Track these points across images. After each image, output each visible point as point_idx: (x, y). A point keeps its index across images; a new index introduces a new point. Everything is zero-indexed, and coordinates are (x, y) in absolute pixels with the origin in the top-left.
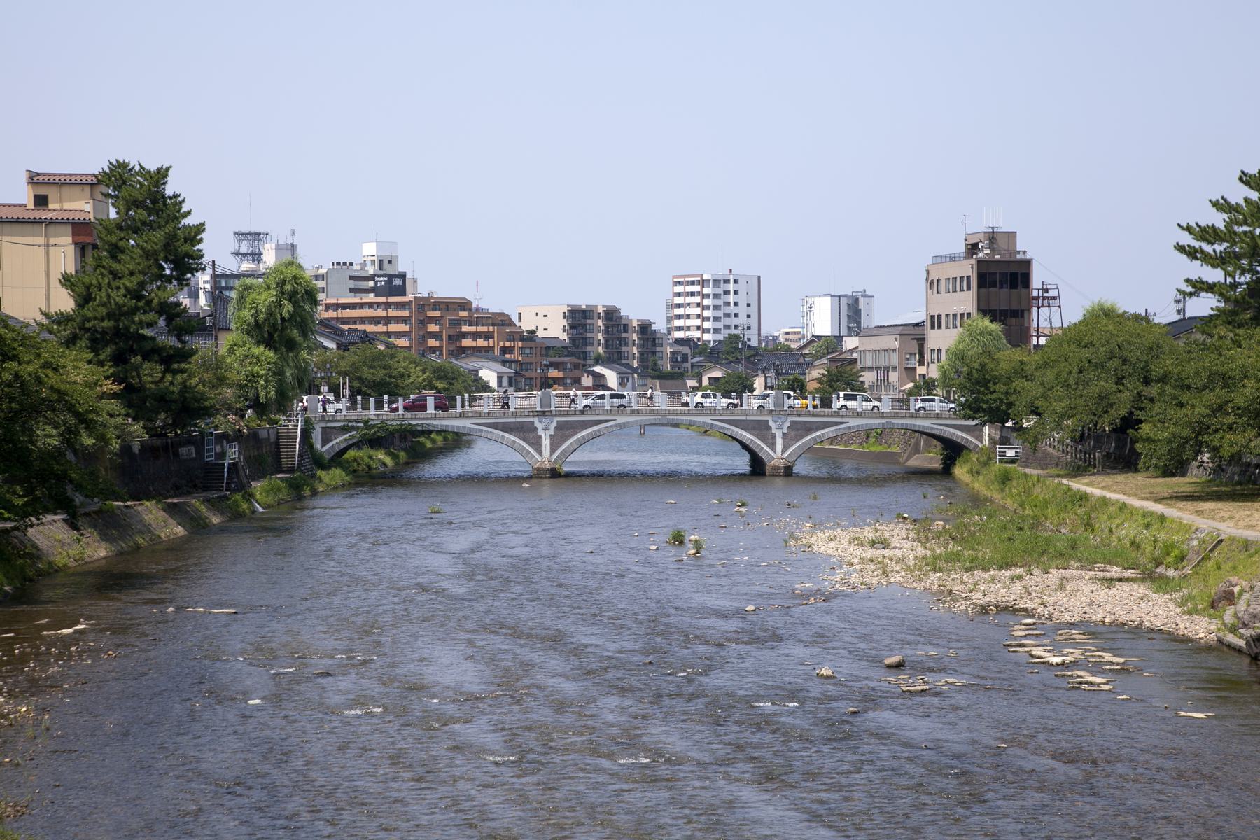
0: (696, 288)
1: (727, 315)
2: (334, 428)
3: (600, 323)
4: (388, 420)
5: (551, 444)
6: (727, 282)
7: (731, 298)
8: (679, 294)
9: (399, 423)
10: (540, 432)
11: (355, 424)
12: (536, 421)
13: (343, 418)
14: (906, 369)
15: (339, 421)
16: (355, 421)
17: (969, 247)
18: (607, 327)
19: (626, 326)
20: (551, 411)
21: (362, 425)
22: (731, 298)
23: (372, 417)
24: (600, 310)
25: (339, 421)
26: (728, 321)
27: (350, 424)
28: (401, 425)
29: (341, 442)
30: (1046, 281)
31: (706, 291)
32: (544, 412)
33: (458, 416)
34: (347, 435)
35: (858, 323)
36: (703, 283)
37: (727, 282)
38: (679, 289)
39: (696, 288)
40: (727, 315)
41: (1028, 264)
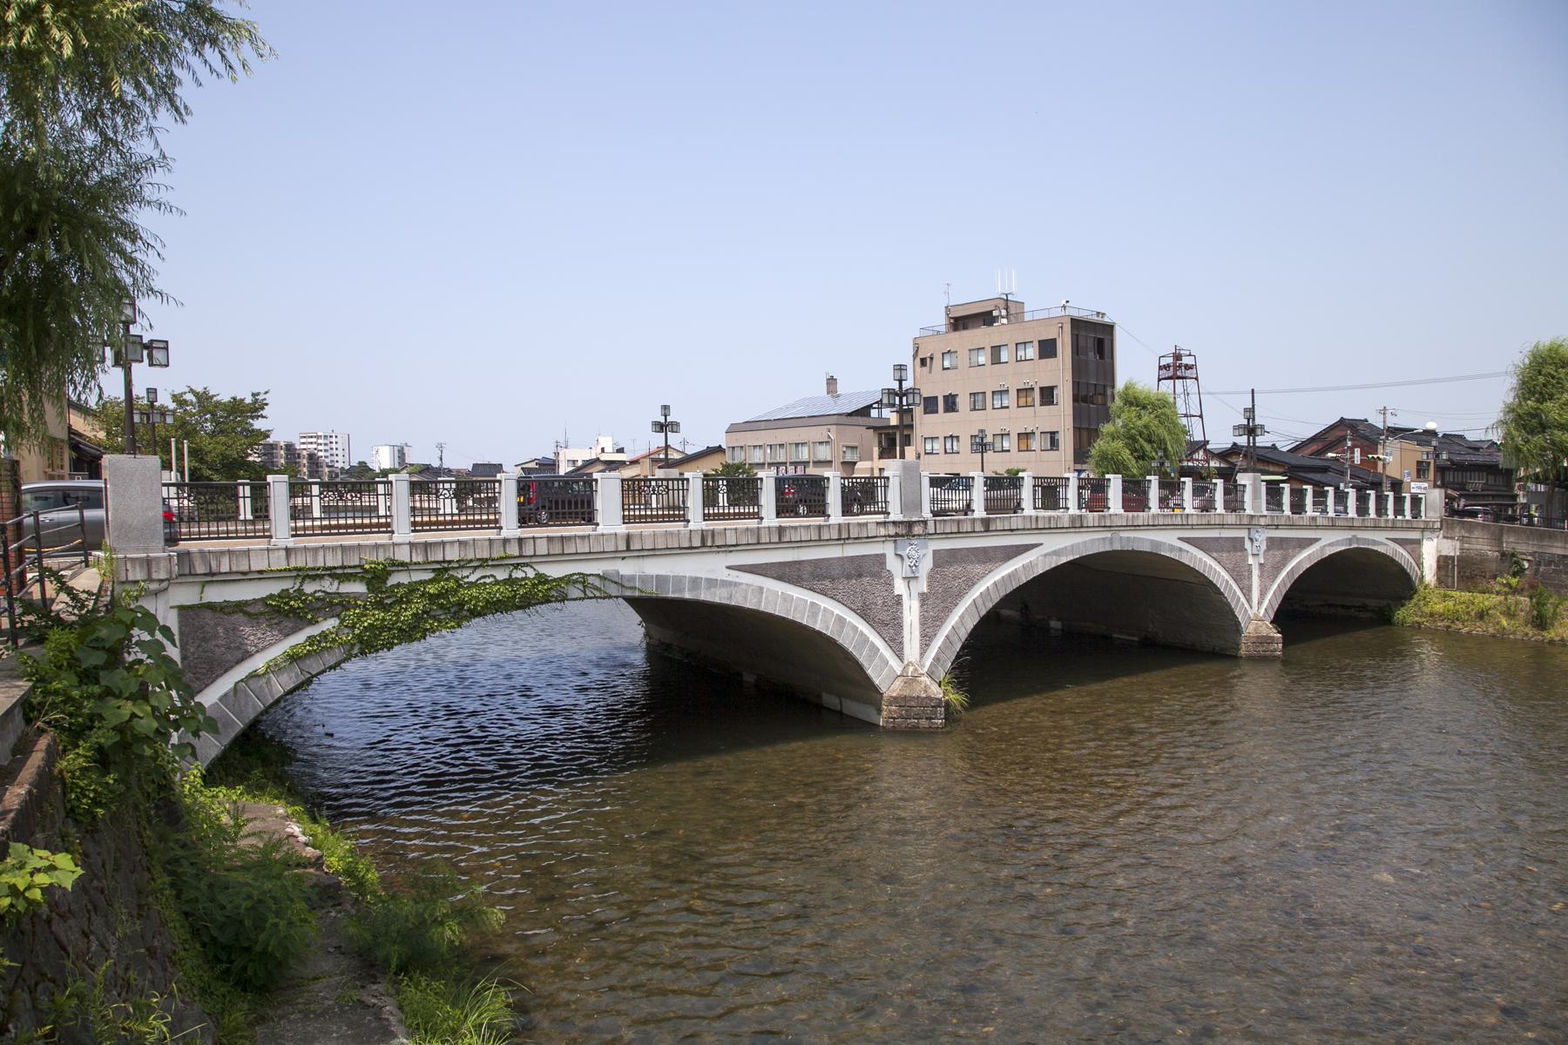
0: (314, 440)
1: (332, 455)
2: (240, 607)
3: (282, 452)
4: (462, 563)
5: (924, 622)
6: (331, 437)
7: (334, 446)
8: (304, 443)
9: (501, 575)
10: (900, 587)
11: (330, 586)
12: (888, 549)
13: (279, 562)
14: (843, 463)
15: (262, 576)
16: (332, 573)
17: (952, 321)
18: (287, 455)
19: (299, 454)
20: (925, 522)
21: (359, 588)
22: (334, 446)
23: (403, 555)
24: (282, 444)
25: (262, 576)
26: (332, 458)
27: (309, 588)
28: (510, 581)
29: (274, 668)
30: (1180, 346)
31: (320, 441)
32: (910, 524)
33: (696, 542)
34: (300, 638)
35: (404, 460)
36: (318, 437)
37: (331, 437)
38: (303, 440)
39: (314, 440)
40: (332, 455)
41: (1110, 328)
